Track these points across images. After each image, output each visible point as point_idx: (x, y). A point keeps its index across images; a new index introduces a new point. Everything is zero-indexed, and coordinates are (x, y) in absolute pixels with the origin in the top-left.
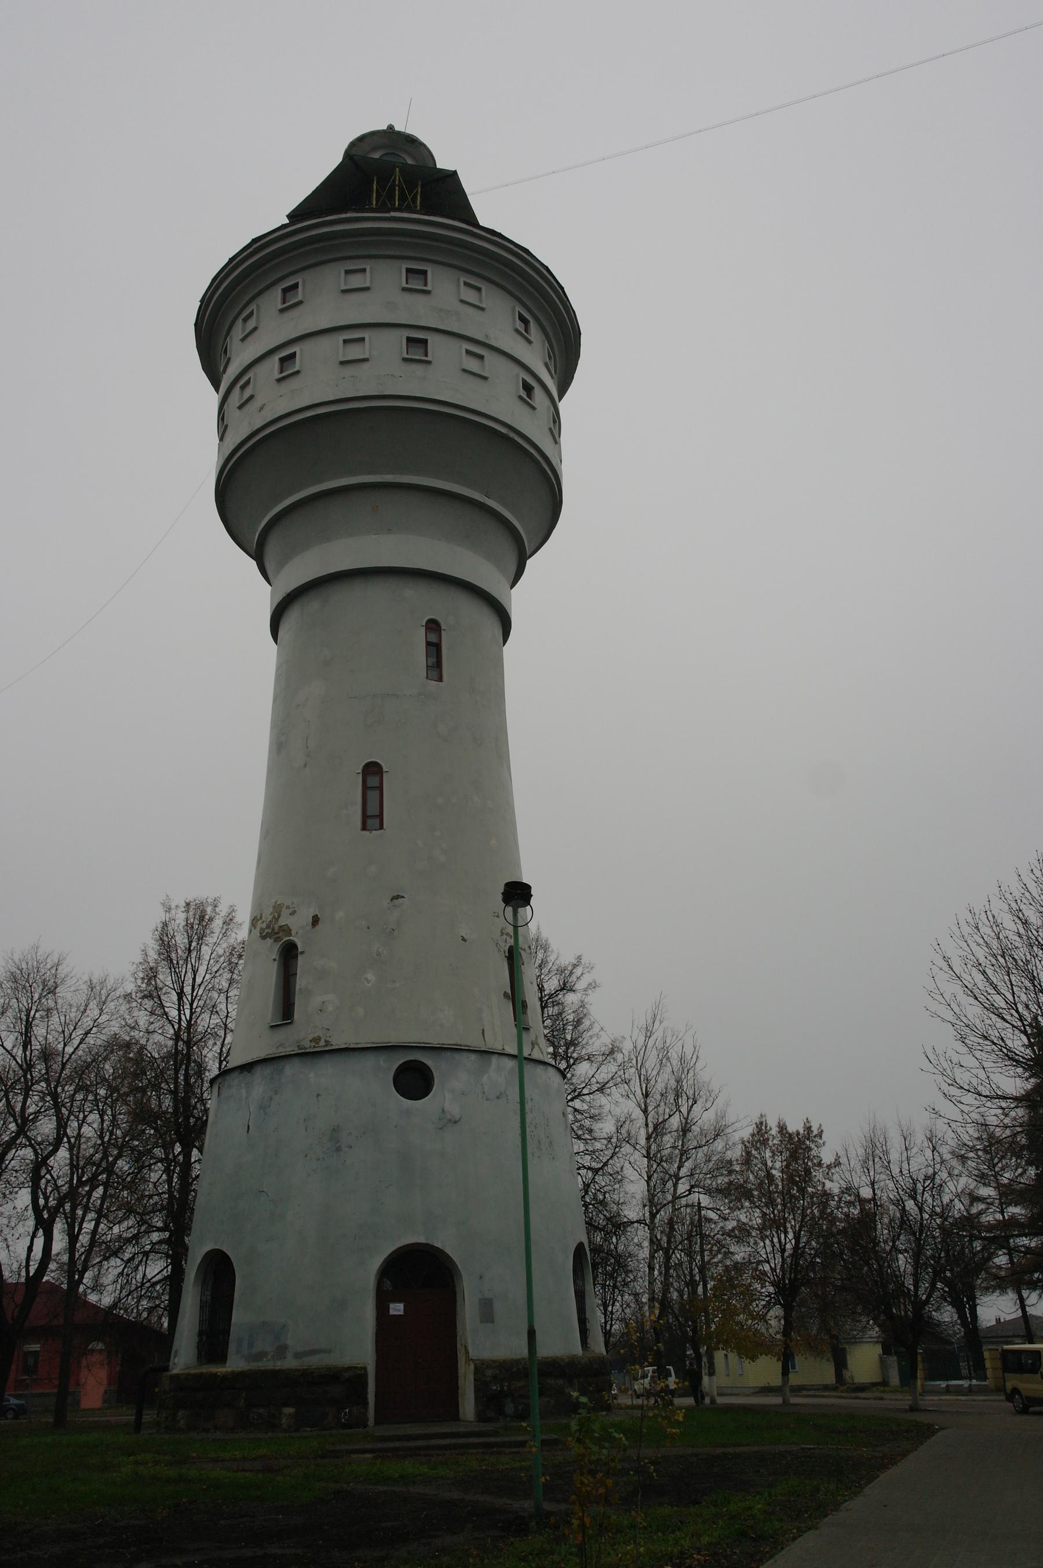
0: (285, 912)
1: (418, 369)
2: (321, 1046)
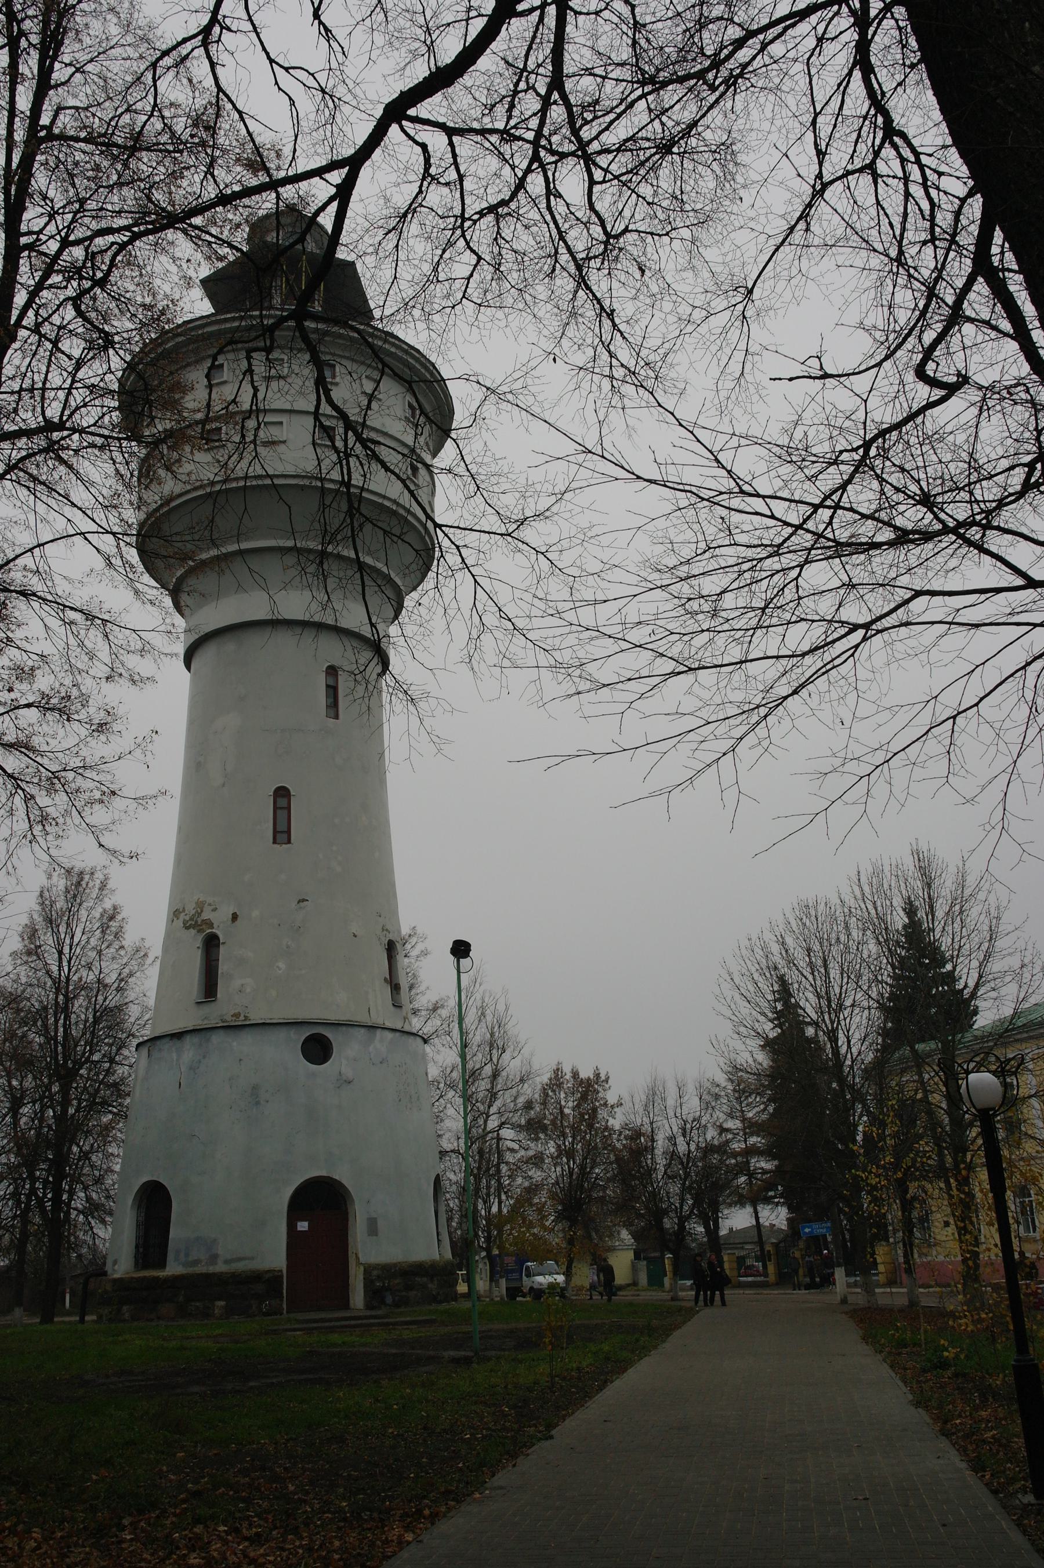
0: (207, 909)
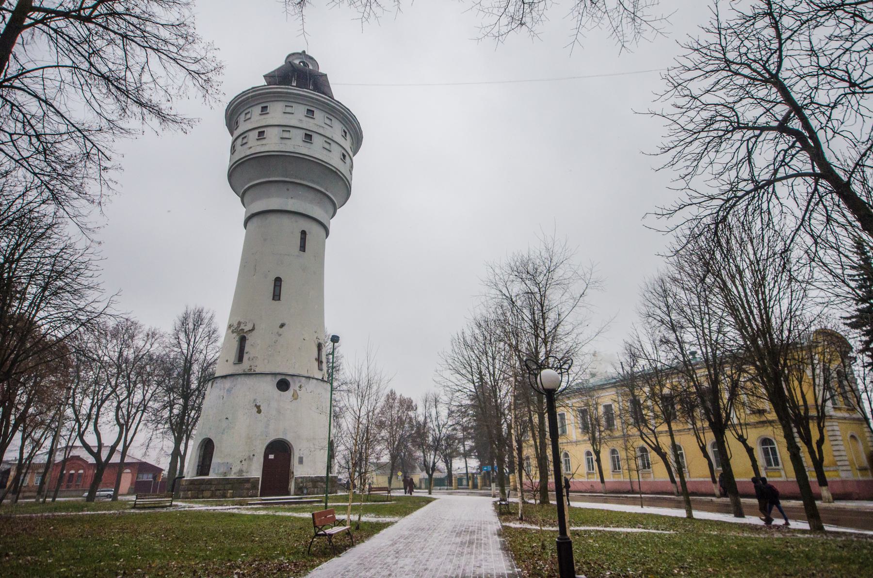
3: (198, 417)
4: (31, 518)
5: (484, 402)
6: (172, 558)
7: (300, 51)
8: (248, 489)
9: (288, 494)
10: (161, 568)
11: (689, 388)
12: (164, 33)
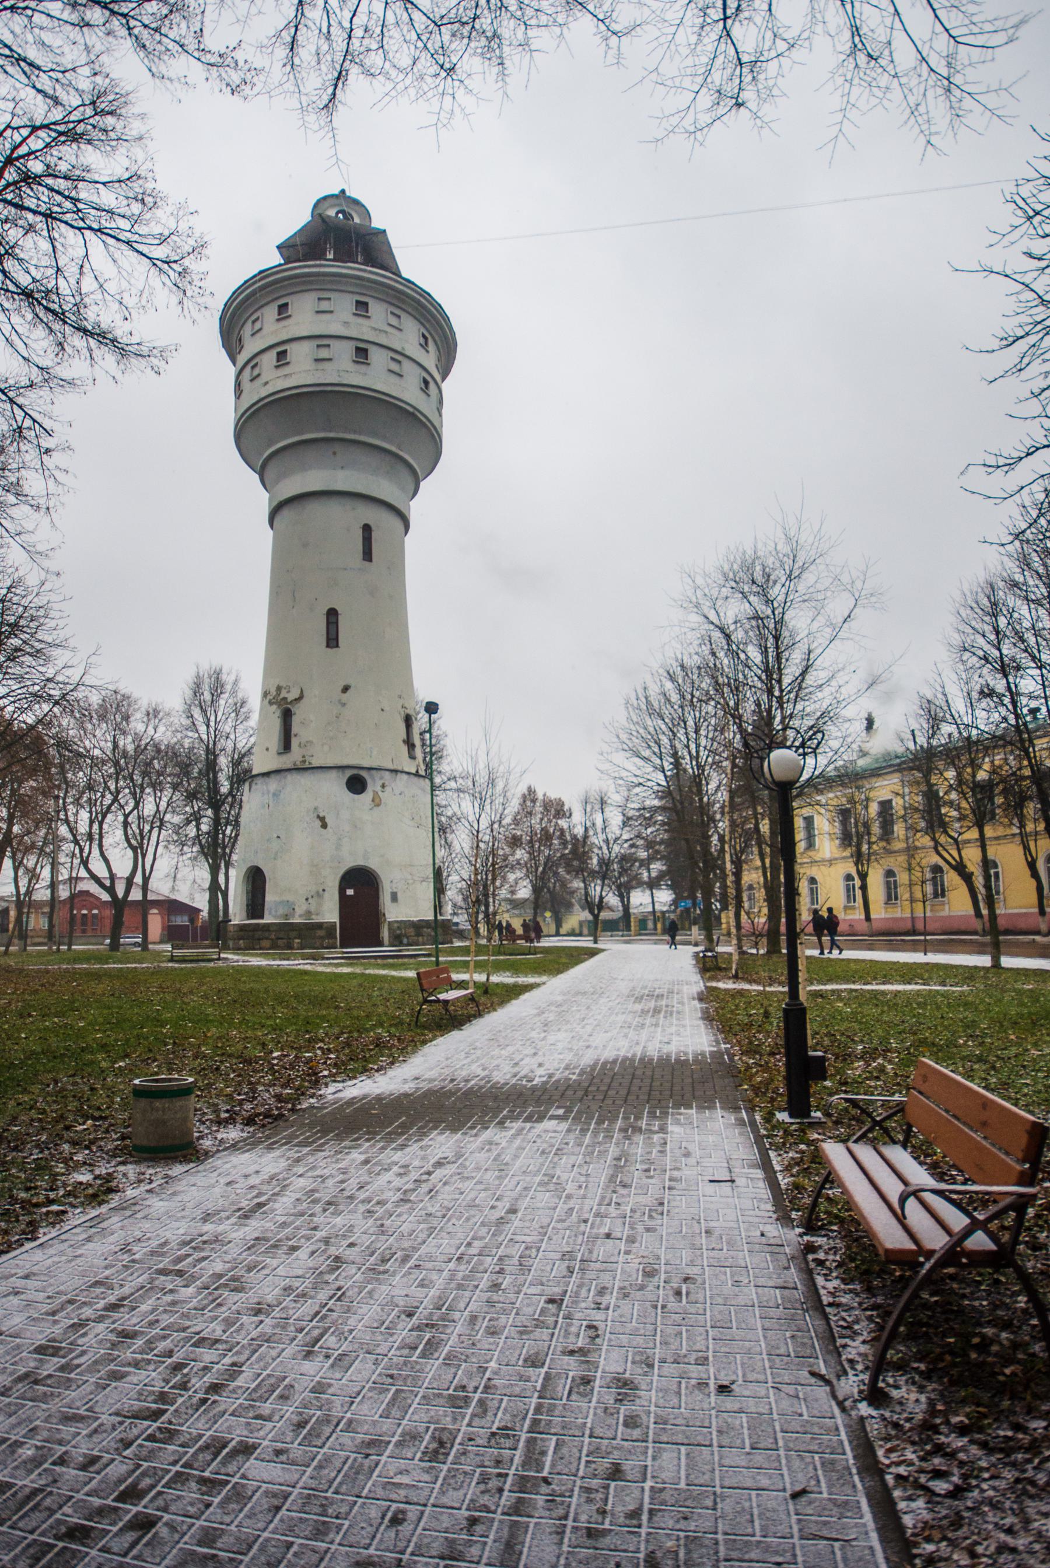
1: (363, 368)
2: (307, 765)
3: (237, 835)
4: (47, 971)
5: (682, 805)
6: (231, 1024)
7: (336, 192)
8: (321, 938)
9: (380, 944)
10: (220, 1038)
11: (1020, 769)
12: (108, 198)
